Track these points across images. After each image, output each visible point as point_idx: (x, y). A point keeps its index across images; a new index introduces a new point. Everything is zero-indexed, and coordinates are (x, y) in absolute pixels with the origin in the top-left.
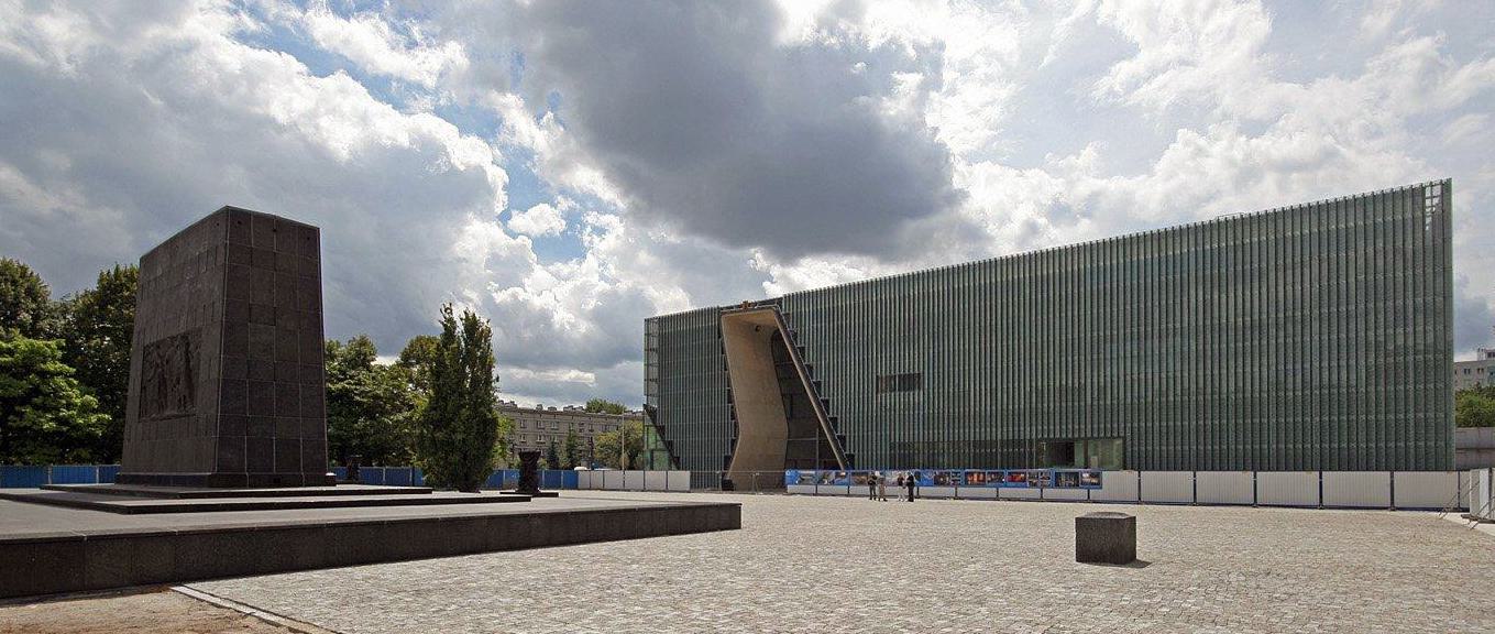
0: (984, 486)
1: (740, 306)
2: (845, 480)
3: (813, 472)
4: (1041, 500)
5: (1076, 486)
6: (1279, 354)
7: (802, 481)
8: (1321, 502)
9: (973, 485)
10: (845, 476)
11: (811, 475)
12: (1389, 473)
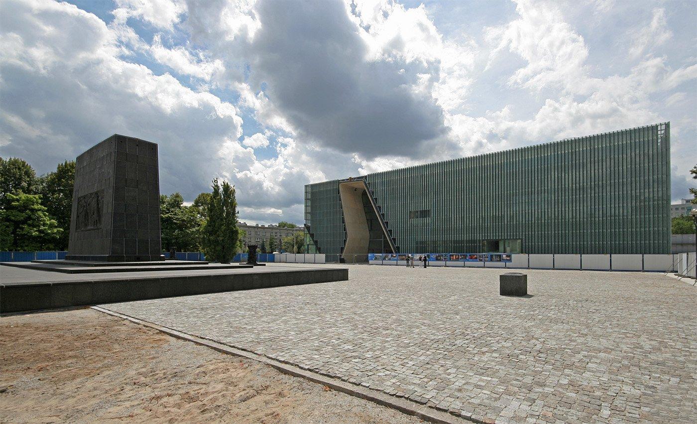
0: (458, 261)
1: (348, 180)
2: (396, 258)
3: (381, 255)
5: (500, 261)
7: (376, 259)
9: (453, 260)
10: (395, 257)
11: (380, 256)
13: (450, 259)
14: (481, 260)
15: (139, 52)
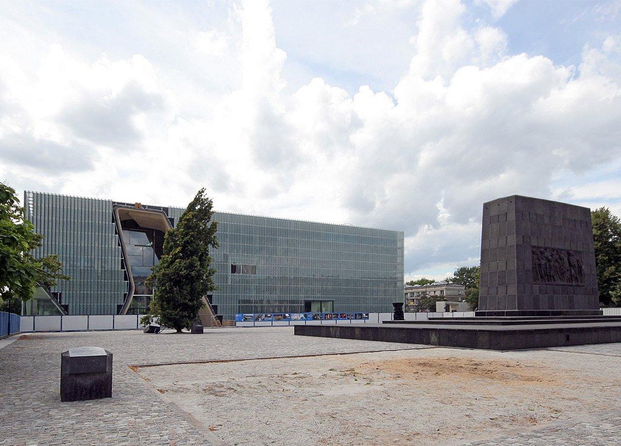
0: (331, 319)
1: (133, 205)
2: (270, 319)
3: (253, 315)
4: (272, 326)
5: (361, 319)
6: (559, 276)
7: (246, 320)
8: (113, 328)
9: (328, 319)
10: (270, 317)
11: (251, 316)
12: (33, 317)
13: (325, 318)
14: (348, 319)
15: (539, 61)
